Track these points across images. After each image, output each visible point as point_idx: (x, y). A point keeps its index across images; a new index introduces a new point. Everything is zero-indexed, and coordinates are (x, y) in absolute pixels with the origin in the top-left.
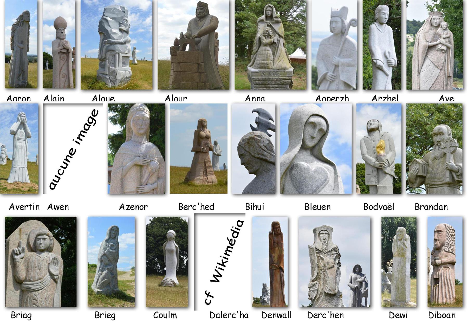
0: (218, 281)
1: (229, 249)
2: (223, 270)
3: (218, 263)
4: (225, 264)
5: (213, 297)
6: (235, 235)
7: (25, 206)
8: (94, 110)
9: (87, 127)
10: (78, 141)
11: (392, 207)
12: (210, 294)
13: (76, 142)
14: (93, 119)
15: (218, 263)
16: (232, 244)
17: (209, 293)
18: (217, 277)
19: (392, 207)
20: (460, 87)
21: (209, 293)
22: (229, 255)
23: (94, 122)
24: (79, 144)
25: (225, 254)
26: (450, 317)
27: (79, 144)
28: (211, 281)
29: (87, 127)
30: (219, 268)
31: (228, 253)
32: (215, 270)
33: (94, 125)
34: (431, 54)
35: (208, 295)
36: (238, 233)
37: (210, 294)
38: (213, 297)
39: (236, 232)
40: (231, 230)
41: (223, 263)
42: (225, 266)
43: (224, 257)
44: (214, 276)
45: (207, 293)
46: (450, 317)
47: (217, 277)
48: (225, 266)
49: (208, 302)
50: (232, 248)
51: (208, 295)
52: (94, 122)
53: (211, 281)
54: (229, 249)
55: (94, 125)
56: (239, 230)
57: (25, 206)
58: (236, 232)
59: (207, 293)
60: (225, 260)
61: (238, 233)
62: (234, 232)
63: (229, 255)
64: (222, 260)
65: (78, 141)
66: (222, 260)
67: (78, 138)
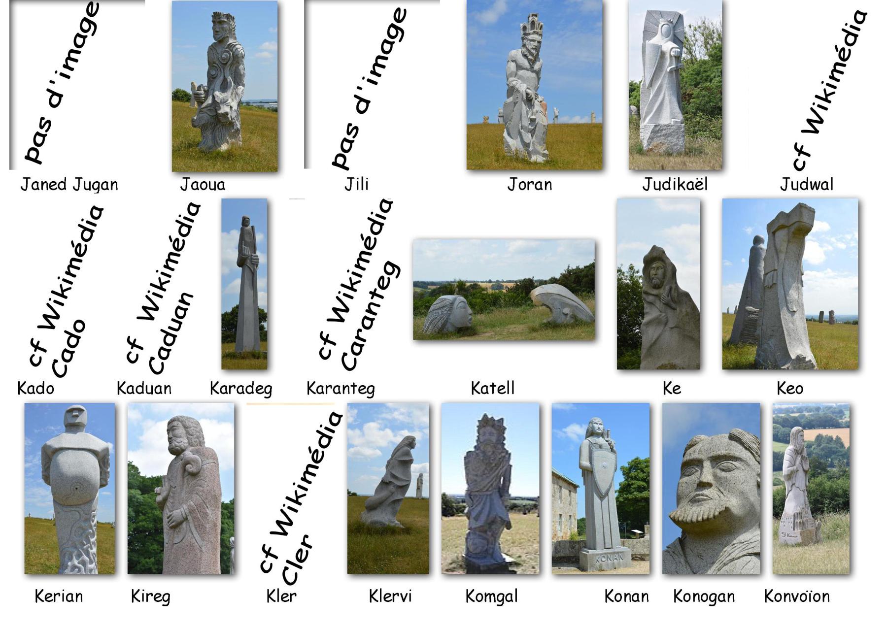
1: (172, 257)
2: (352, 298)
3: (53, 292)
5: (142, 348)
7: (394, 595)
8: (398, 10)
9: (80, 41)
10: (66, 72)
11: (506, 390)
12: (136, 343)
13: (369, 80)
14: (89, 22)
15: (151, 285)
16: (178, 247)
17: (135, 340)
18: (340, 313)
19: (506, 390)
21: (135, 340)
22: (173, 270)
23: (400, 33)
24: (68, 77)
25: (66, 273)
26: (107, 189)
27: (68, 77)
28: (138, 318)
29: (80, 41)
33: (93, 35)
35: (133, 345)
36: (189, 227)
37: (136, 343)
38: (142, 348)
43: (162, 273)
46: (107, 189)
47: (340, 313)
48: (355, 290)
49: (132, 357)
50: (317, 467)
51: (133, 345)
52: (400, 33)
53: (138, 318)
54: (172, 257)
55: (93, 35)
56: (192, 221)
57: (394, 595)
59: (132, 341)
60: (829, 90)
61: (189, 227)
63: (173, 270)
64: (350, 279)
65: (66, 72)
67: (165, 266)
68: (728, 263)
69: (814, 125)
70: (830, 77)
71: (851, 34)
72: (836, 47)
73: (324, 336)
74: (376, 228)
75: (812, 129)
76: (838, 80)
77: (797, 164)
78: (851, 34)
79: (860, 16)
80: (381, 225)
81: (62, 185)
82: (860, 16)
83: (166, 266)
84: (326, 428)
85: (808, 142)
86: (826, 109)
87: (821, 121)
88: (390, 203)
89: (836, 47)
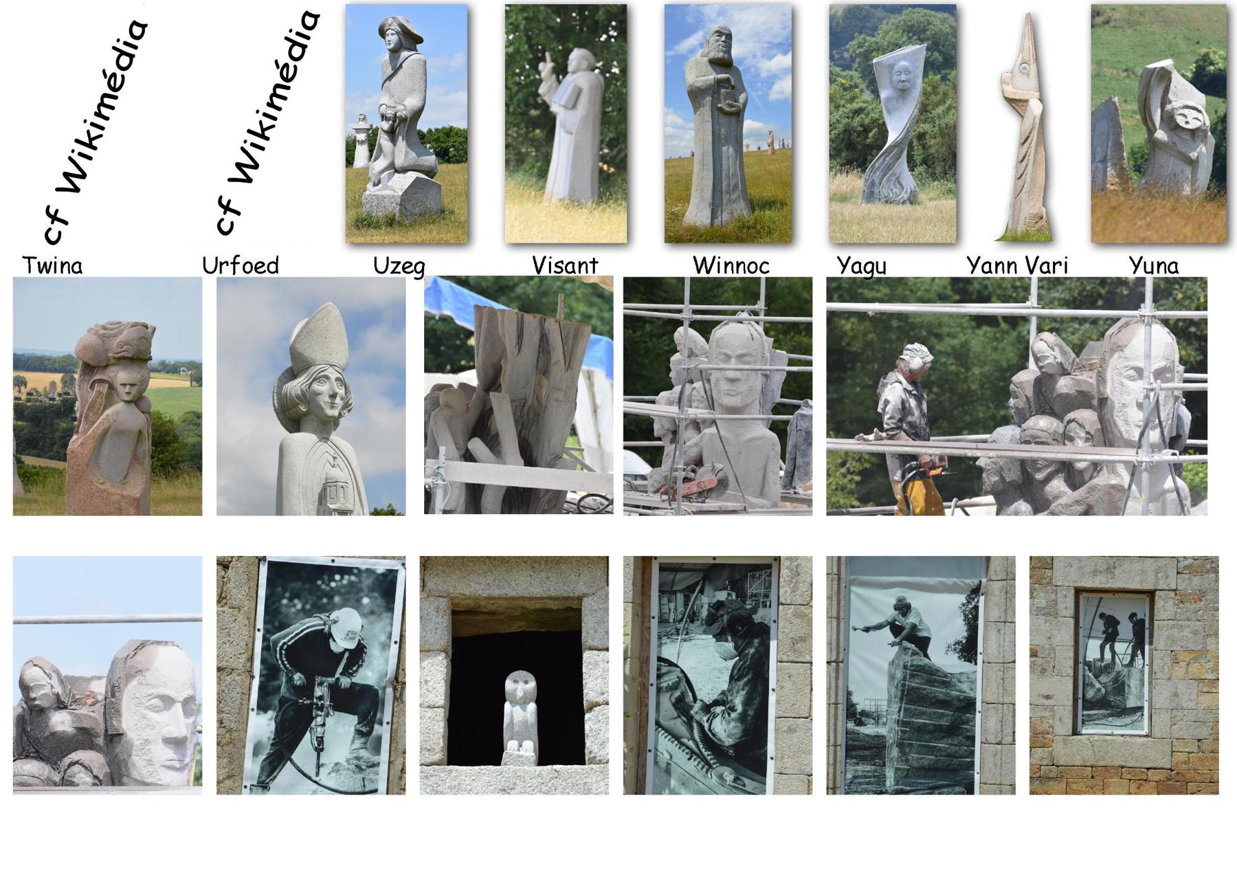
0: (77, 190)
1: (279, 91)
2: (263, 149)
4: (95, 143)
6: (124, 61)
16: (287, 76)
17: (57, 211)
18: (246, 169)
20: (39, 381)
21: (57, 211)
25: (268, 105)
30: (80, 154)
31: (277, 101)
32: (70, 158)
34: (442, 730)
39: (298, 44)
40: (286, 38)
41: (263, 130)
42: (95, 148)
44: (239, 166)
45: (52, 212)
47: (246, 169)
48: (267, 139)
54: (279, 91)
58: (298, 44)
59: (52, 212)
60: (267, 122)
62: (295, 43)
64: (261, 122)
66: (261, 122)
68: (449, 367)
69: (73, 181)
70: (96, 114)
71: (125, 55)
72: (104, 71)
73: (224, 202)
74: (297, 51)
75: (243, 177)
76: (107, 118)
77: (50, 235)
78: (125, 55)
79: (138, 29)
80: (304, 47)
81: (273, 267)
82: (138, 29)
83: (271, 105)
84: (126, 43)
85: (238, 194)
86: (90, 158)
87: (83, 176)
88: (316, 17)
89: (104, 71)
